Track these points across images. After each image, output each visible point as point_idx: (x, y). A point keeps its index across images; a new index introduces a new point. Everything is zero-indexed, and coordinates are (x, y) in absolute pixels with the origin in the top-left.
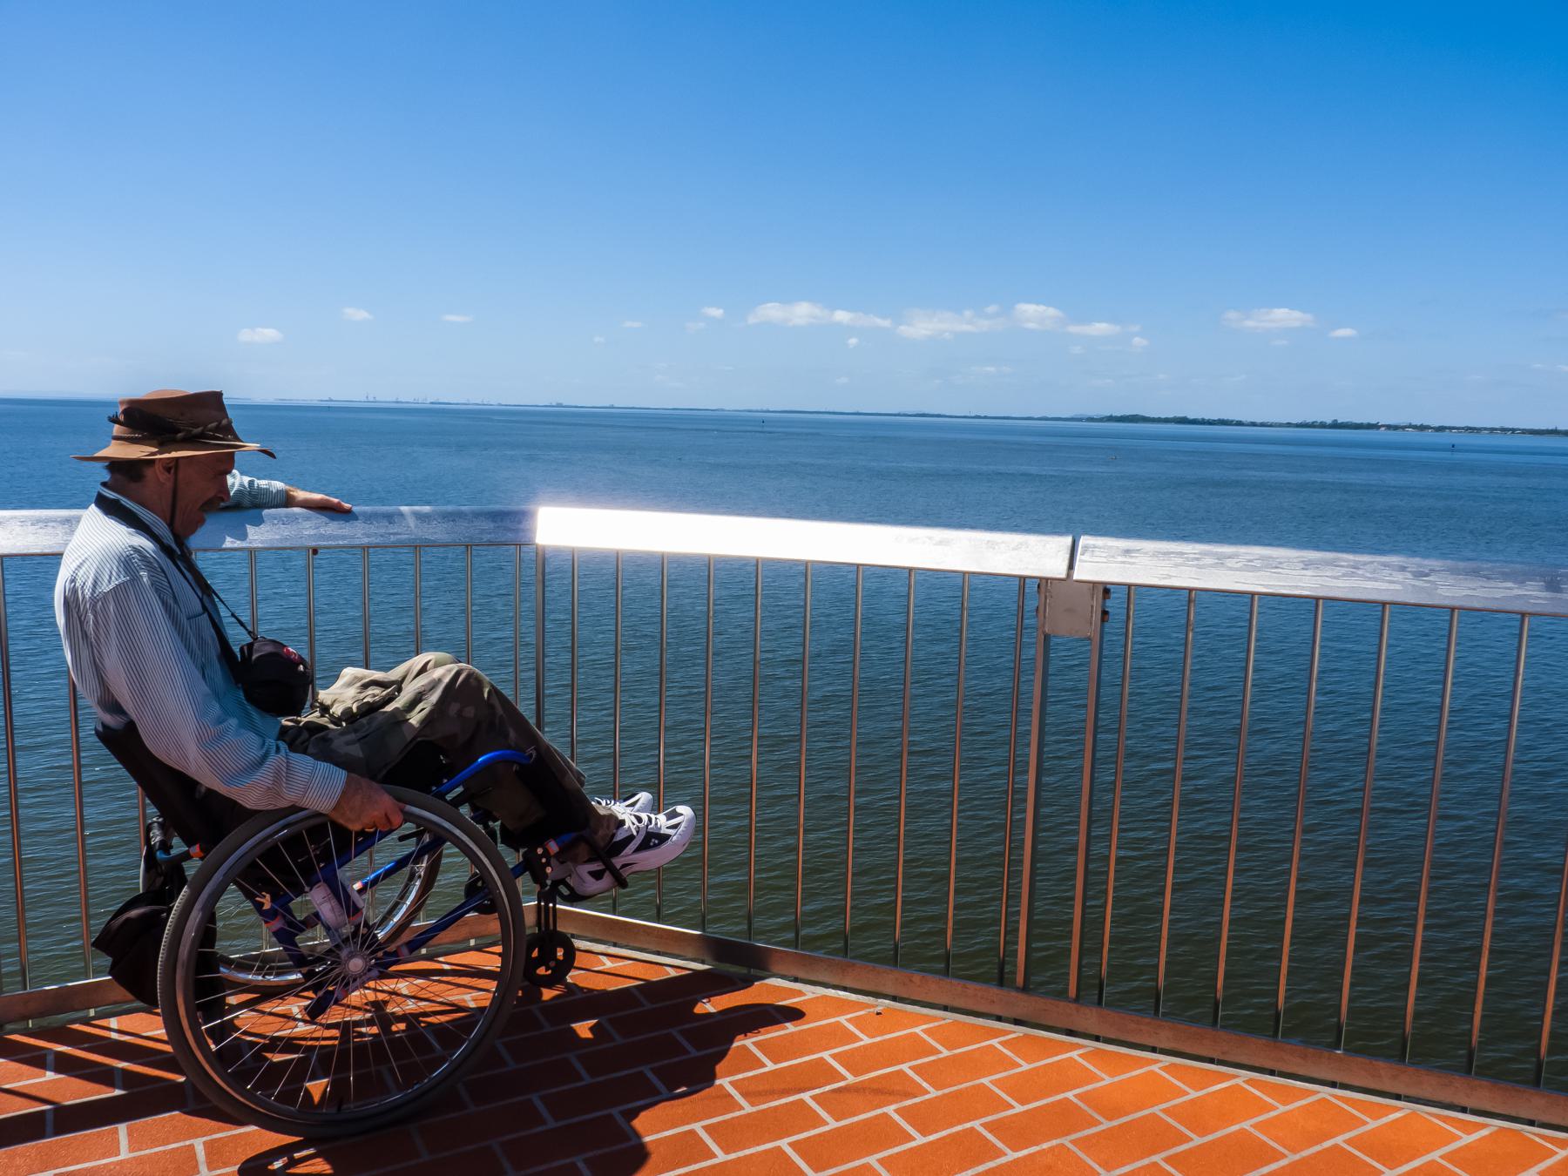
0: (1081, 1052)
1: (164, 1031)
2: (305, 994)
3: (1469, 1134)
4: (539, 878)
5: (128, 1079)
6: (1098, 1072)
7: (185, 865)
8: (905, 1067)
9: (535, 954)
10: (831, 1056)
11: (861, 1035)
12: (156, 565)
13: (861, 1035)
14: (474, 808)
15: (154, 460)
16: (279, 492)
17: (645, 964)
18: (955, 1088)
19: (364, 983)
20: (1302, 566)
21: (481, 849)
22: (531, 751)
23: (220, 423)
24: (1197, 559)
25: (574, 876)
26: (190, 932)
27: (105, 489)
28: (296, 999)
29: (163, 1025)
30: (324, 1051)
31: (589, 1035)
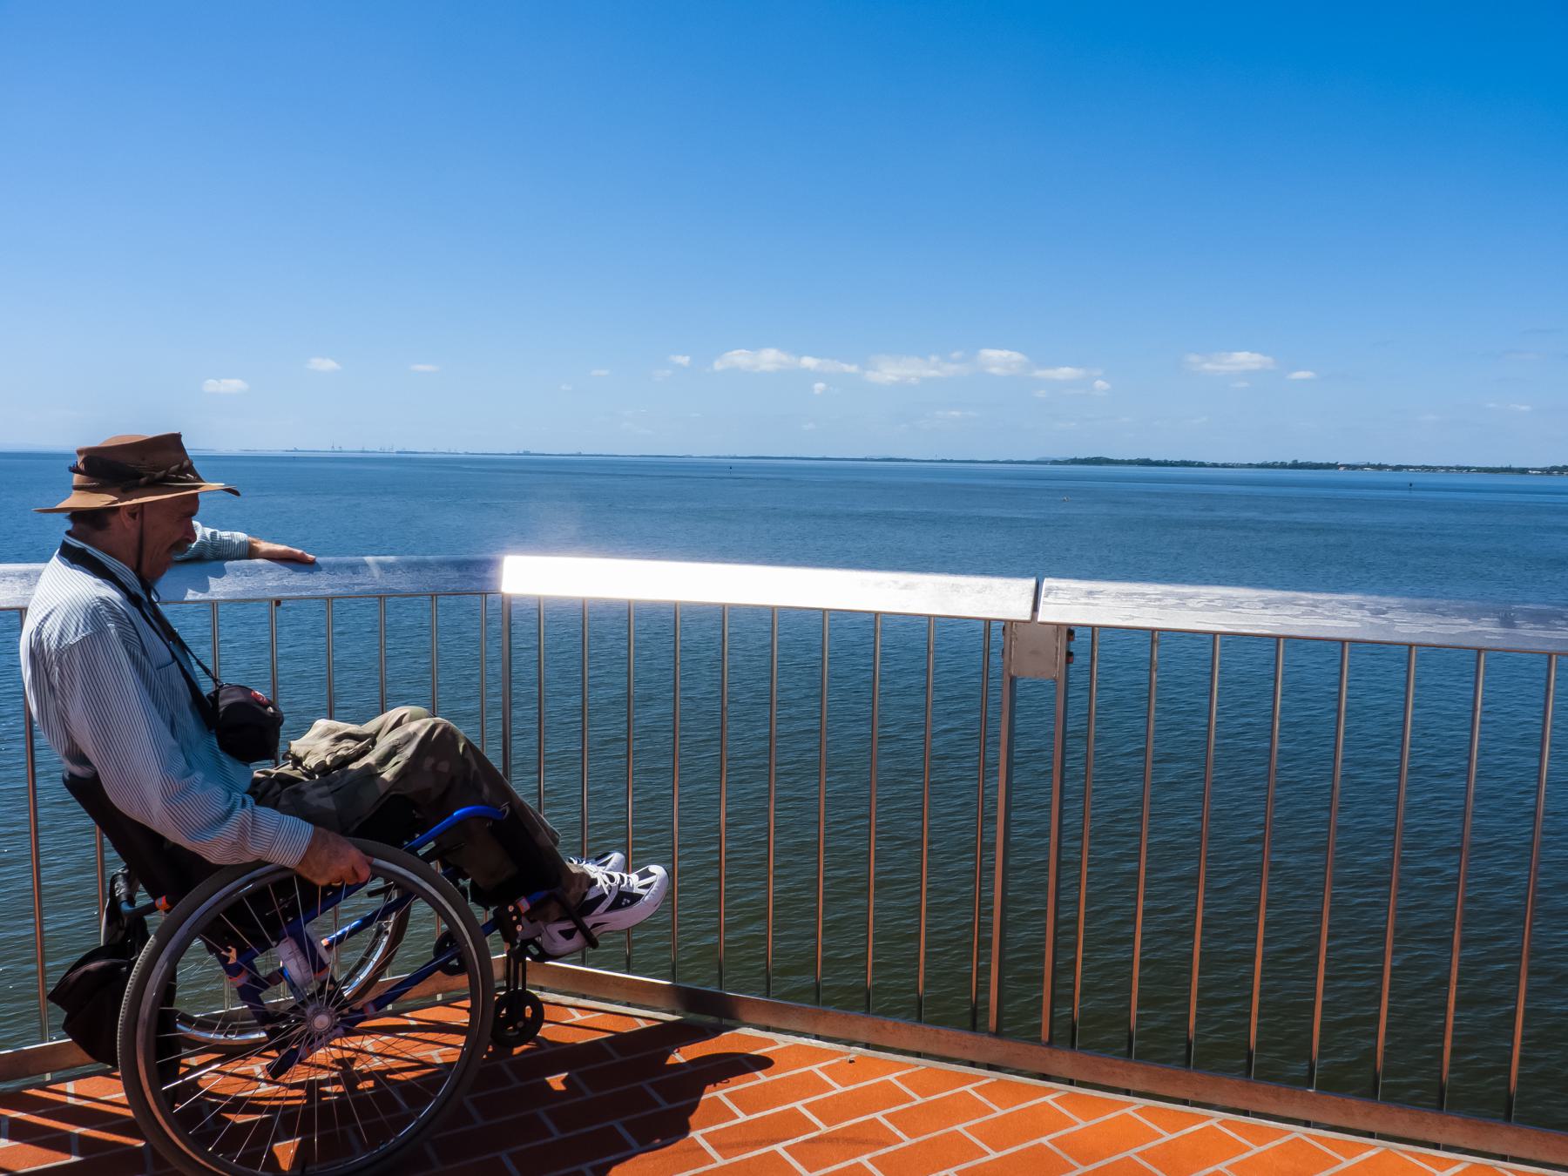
1: (124, 1094)
2: (267, 1053)
4: (509, 936)
5: (85, 1144)
8: (878, 1116)
12: (124, 616)
14: (445, 865)
15: (118, 508)
16: (241, 543)
17: (615, 1016)
18: (929, 1136)
19: (330, 1040)
20: (1262, 605)
22: (505, 807)
23: (182, 464)
24: (1159, 600)
25: (545, 935)
27: (70, 538)
29: (123, 1088)
30: (287, 1112)
31: (562, 1088)
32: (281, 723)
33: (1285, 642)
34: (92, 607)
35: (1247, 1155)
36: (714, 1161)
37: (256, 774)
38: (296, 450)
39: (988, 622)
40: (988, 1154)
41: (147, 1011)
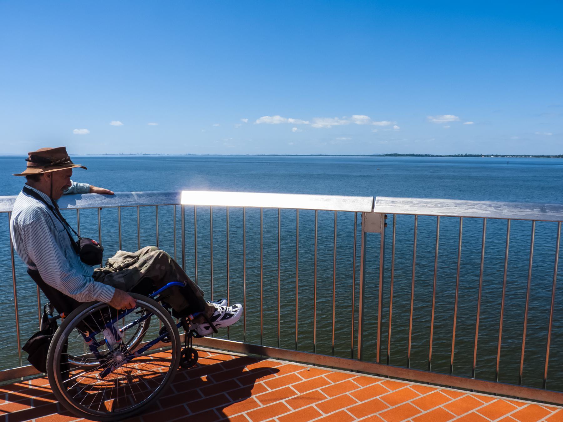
0: (381, 382)
1: (49, 384)
2: (100, 370)
3: (520, 407)
4: (186, 328)
5: (36, 402)
6: (387, 389)
7: (57, 321)
8: (318, 389)
9: (184, 356)
10: (292, 386)
11: (302, 378)
12: (47, 214)
13: (302, 378)
14: (163, 303)
15: (44, 173)
16: (87, 187)
19: (122, 365)
20: (455, 205)
21: (164, 315)
23: (66, 158)
24: (418, 204)
26: (58, 348)
28: (97, 371)
29: (49, 382)
31: (206, 380)
32: (103, 251)
33: (463, 218)
34: (35, 210)
35: (451, 402)
36: (260, 406)
37: (95, 270)
38: (107, 155)
39: (356, 213)
40: (358, 402)
41: (57, 354)
